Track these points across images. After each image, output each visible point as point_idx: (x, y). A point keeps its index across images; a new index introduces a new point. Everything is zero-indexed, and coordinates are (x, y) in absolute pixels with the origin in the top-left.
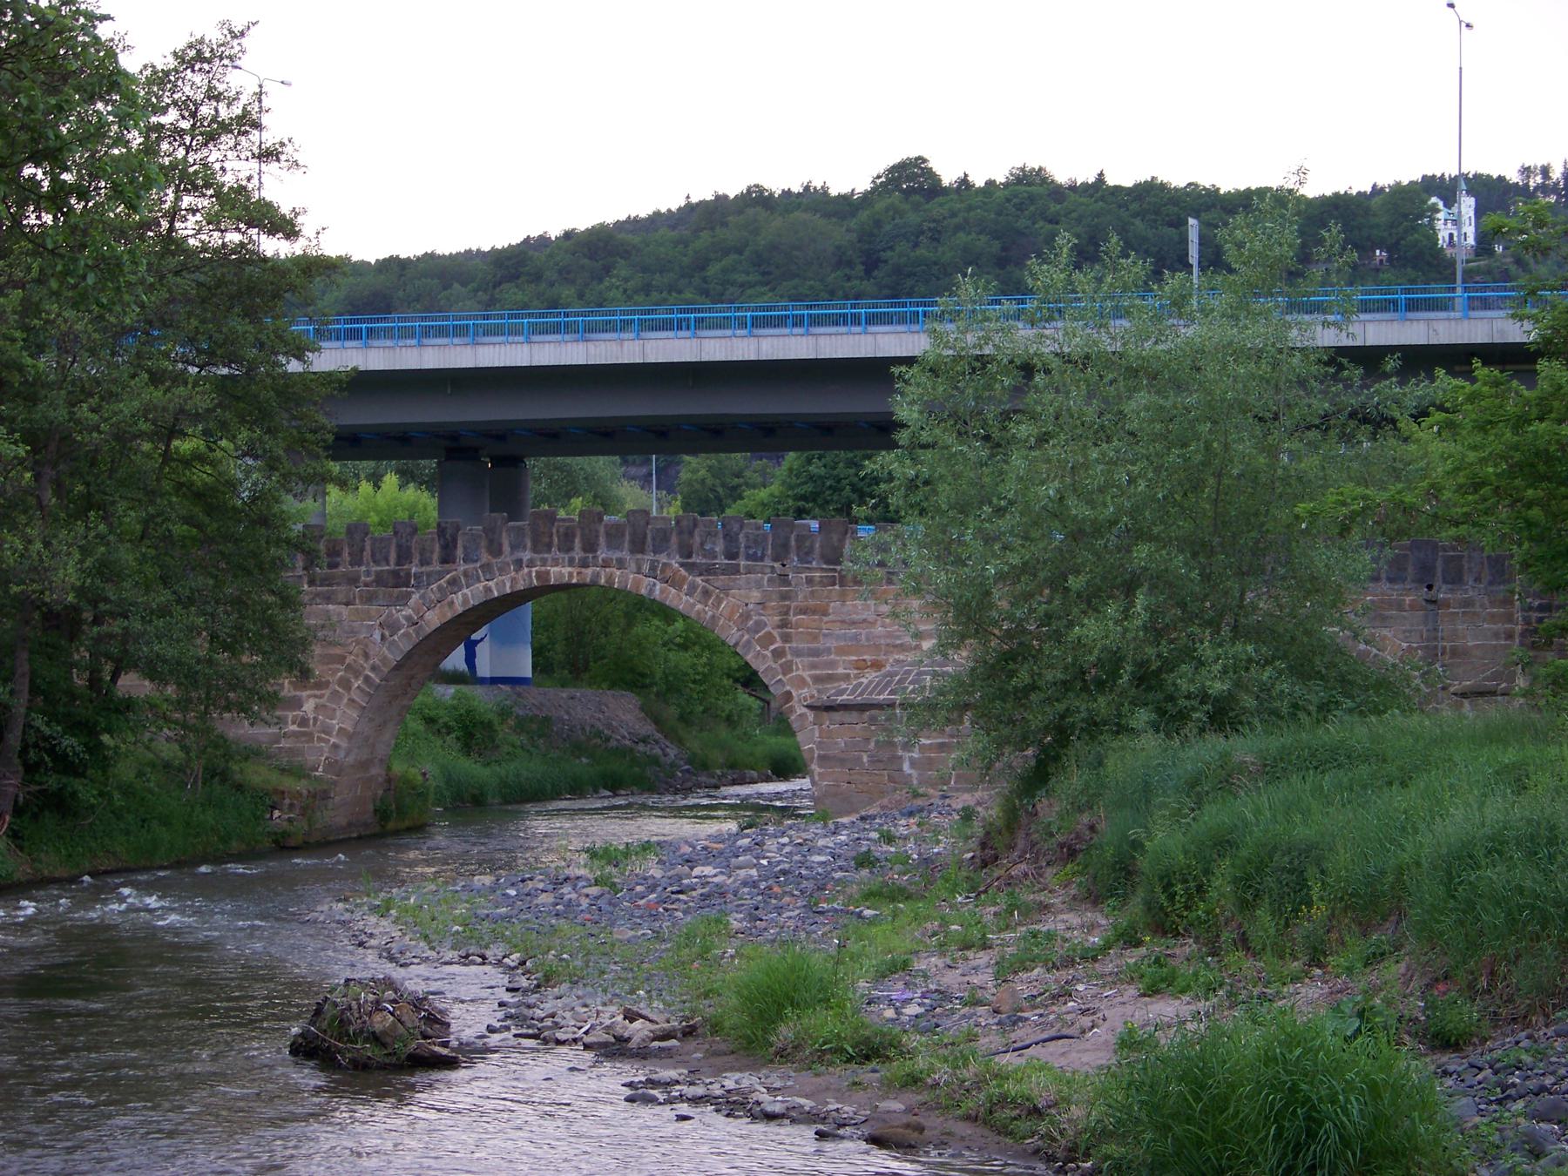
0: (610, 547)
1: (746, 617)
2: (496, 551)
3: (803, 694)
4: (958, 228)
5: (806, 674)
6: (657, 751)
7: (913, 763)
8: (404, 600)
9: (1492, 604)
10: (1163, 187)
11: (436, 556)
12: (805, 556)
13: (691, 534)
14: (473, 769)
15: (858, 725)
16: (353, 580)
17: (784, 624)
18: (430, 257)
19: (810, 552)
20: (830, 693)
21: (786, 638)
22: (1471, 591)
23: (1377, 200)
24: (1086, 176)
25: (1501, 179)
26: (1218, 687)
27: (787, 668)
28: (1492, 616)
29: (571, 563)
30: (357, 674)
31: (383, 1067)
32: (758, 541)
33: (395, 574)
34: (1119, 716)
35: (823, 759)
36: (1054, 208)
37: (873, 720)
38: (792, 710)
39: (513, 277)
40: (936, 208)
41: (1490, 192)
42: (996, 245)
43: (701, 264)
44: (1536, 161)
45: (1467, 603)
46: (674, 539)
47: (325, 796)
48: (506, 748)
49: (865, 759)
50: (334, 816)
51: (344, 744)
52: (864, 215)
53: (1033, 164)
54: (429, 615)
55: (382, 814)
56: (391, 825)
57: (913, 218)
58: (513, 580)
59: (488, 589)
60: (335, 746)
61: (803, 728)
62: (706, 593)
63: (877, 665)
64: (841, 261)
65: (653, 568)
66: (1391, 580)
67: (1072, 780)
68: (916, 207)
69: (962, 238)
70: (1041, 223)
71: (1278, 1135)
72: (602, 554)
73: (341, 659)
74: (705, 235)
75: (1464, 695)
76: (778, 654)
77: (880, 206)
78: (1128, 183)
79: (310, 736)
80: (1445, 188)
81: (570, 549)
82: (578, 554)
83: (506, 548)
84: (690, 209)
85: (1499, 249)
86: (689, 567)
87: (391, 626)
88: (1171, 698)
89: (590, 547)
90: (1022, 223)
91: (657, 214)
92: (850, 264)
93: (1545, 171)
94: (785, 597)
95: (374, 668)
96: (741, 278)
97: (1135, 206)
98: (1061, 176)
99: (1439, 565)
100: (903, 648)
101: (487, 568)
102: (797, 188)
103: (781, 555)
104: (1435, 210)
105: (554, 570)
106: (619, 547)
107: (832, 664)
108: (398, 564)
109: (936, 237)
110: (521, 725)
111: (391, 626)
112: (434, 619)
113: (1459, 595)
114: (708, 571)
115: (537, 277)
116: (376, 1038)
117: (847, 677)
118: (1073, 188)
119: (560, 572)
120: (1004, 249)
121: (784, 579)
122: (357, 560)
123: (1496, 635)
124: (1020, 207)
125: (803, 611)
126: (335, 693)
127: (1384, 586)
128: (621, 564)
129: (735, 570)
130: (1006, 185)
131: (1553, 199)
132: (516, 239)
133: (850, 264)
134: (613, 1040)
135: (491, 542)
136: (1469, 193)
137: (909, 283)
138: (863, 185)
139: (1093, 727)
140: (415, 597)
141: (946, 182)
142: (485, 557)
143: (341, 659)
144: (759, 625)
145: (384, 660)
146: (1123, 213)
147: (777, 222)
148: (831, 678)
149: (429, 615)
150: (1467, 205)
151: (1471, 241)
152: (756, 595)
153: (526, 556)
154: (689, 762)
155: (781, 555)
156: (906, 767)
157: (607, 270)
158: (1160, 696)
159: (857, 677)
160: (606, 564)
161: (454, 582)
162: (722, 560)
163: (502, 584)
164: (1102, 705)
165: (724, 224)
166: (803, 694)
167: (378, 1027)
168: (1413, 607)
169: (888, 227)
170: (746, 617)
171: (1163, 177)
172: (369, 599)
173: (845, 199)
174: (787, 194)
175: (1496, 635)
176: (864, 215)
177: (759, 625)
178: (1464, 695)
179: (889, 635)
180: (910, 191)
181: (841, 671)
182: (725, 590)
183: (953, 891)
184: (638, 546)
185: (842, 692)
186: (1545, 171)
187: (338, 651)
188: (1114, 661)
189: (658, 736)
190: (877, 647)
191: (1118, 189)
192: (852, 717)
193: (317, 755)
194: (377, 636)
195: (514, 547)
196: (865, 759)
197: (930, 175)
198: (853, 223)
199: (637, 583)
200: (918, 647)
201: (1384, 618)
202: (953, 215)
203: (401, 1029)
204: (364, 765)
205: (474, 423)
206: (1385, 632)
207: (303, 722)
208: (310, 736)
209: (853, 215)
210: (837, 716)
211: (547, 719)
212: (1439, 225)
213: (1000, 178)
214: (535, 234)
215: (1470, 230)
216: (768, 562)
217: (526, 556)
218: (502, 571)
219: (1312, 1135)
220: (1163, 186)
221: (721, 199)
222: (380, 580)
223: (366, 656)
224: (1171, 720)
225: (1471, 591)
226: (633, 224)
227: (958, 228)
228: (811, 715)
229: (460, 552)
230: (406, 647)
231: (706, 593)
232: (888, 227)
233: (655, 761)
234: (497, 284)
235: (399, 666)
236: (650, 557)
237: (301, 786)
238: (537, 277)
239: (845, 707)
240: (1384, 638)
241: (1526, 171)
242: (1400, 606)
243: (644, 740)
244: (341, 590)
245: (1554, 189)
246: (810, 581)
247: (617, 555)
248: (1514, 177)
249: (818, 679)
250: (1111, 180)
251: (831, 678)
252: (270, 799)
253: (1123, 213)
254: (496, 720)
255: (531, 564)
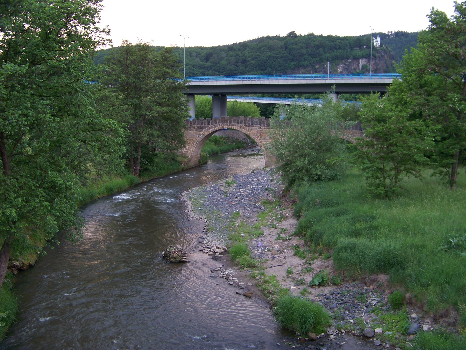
0: (234, 123)
1: (255, 134)
2: (216, 123)
4: (300, 43)
6: (246, 141)
8: (202, 130)
10: (331, 36)
11: (207, 124)
12: (264, 124)
13: (246, 121)
14: (216, 148)
16: (194, 128)
17: (260, 135)
18: (219, 46)
19: (264, 124)
21: (261, 137)
23: (365, 38)
24: (319, 34)
25: (385, 33)
26: (319, 173)
27: (261, 142)
29: (228, 125)
30: (195, 142)
31: (175, 263)
32: (256, 122)
33: (200, 127)
34: (303, 177)
36: (314, 39)
39: (231, 50)
40: (296, 39)
41: (382, 36)
42: (306, 45)
43: (260, 48)
44: (391, 31)
46: (243, 122)
47: (190, 161)
48: (221, 144)
50: (192, 164)
51: (193, 153)
52: (285, 40)
53: (311, 32)
54: (206, 133)
55: (200, 162)
56: (201, 163)
57: (293, 41)
58: (219, 128)
59: (215, 129)
60: (192, 153)
62: (248, 130)
64: (282, 48)
65: (240, 126)
66: (355, 129)
67: (295, 188)
68: (293, 39)
69: (300, 44)
70: (312, 42)
71: (300, 322)
72: (232, 124)
73: (192, 140)
74: (261, 44)
76: (260, 140)
77: (288, 39)
78: (326, 35)
79: (188, 151)
80: (375, 35)
81: (227, 123)
82: (229, 124)
83: (218, 123)
84: (259, 39)
85: (384, 46)
86: (246, 126)
87: (200, 135)
88: (311, 174)
89: (230, 123)
90: (310, 42)
91: (254, 39)
92: (283, 48)
93: (392, 32)
94: (261, 131)
95: (197, 141)
96: (266, 50)
97: (327, 39)
98: (316, 34)
101: (215, 126)
102: (275, 35)
103: (260, 124)
104: (374, 39)
105: (225, 126)
106: (235, 123)
108: (201, 125)
109: (296, 44)
110: (225, 138)
111: (200, 135)
112: (206, 134)
114: (249, 126)
115: (235, 50)
116: (174, 258)
118: (317, 36)
119: (226, 127)
120: (307, 46)
121: (260, 128)
122: (194, 124)
124: (309, 39)
125: (263, 133)
126: (192, 145)
127: (354, 130)
128: (235, 125)
129: (253, 126)
130: (307, 36)
131: (393, 36)
132: (232, 43)
133: (283, 48)
134: (213, 253)
135: (215, 122)
136: (379, 37)
137: (292, 51)
138: (285, 35)
139: (299, 179)
140: (204, 130)
141: (298, 35)
142: (214, 124)
143: (192, 140)
144: (257, 135)
145: (199, 140)
146: (325, 40)
147: (272, 42)
149: (206, 133)
150: (379, 39)
151: (379, 44)
152: (256, 130)
153: (221, 124)
154: (251, 142)
155: (260, 124)
157: (246, 49)
158: (310, 173)
160: (233, 125)
161: (209, 128)
162: (251, 125)
163: (216, 128)
164: (300, 175)
165: (263, 42)
167: (175, 256)
169: (289, 42)
170: (255, 134)
171: (331, 35)
172: (196, 130)
173: (282, 38)
174: (274, 36)
176: (285, 40)
177: (257, 135)
180: (292, 36)
182: (251, 130)
183: (276, 206)
184: (238, 123)
186: (392, 32)
187: (192, 138)
188: (303, 168)
189: (247, 138)
191: (324, 36)
193: (189, 155)
194: (198, 136)
195: (219, 123)
197: (295, 34)
198: (283, 42)
199: (238, 128)
202: (299, 40)
203: (178, 256)
204: (196, 155)
207: (187, 149)
208: (188, 151)
209: (283, 40)
211: (229, 137)
212: (374, 42)
213: (306, 35)
214: (235, 43)
215: (379, 43)
216: (258, 125)
217: (221, 124)
218: (217, 126)
219: (305, 323)
220: (331, 36)
221: (263, 37)
222: (198, 128)
223: (196, 139)
224: (311, 179)
226: (250, 41)
227: (300, 43)
229: (210, 123)
230: (202, 138)
231: (248, 130)
232: (289, 42)
233: (245, 143)
234: (229, 51)
235: (201, 141)
236: (240, 124)
237: (186, 160)
238: (235, 50)
241: (389, 32)
242: (357, 133)
243: (244, 139)
244: (192, 129)
245: (393, 35)
246: (264, 128)
247: (234, 124)
248: (387, 33)
250: (323, 35)
252: (181, 162)
253: (325, 40)
254: (220, 140)
255: (221, 125)
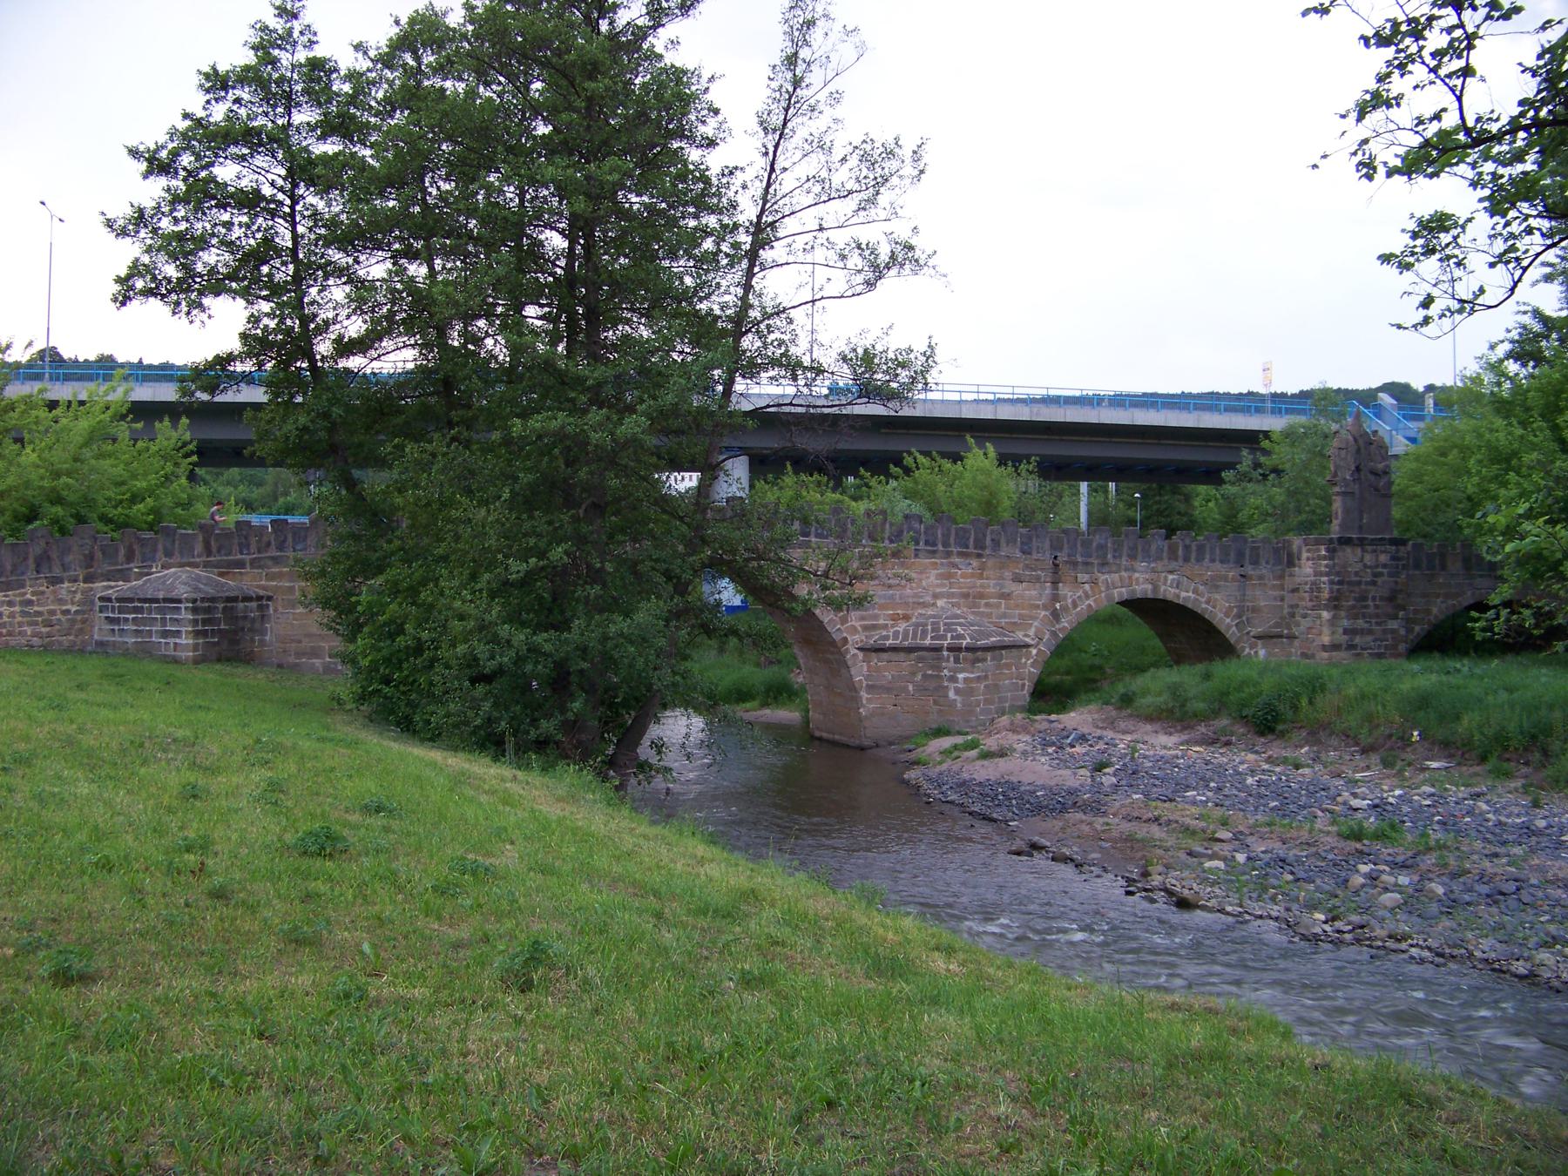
3: (856, 639)
5: (857, 624)
7: (957, 691)
9: (1275, 578)
15: (906, 663)
20: (874, 639)
22: (1264, 570)
28: (1274, 585)
35: (870, 688)
37: (920, 659)
38: (847, 651)
45: (1261, 578)
49: (911, 688)
61: (855, 664)
63: (906, 618)
66: (1222, 562)
75: (1258, 637)
99: (1247, 552)
100: (924, 605)
107: (876, 617)
113: (1258, 572)
117: (885, 627)
123: (1275, 599)
148: (874, 627)
156: (951, 694)
159: (893, 626)
166: (856, 639)
168: (1233, 580)
175: (1275, 599)
178: (1258, 637)
179: (916, 595)
181: (881, 622)
185: (887, 638)
190: (907, 604)
192: (902, 656)
196: (911, 688)
200: (934, 605)
201: (1217, 587)
205: (221, 440)
206: (1217, 596)
210: (885, 656)
225: (1264, 570)
228: (861, 655)
239: (894, 649)
240: (1216, 600)
242: (1225, 579)
249: (866, 628)
251: (874, 627)
